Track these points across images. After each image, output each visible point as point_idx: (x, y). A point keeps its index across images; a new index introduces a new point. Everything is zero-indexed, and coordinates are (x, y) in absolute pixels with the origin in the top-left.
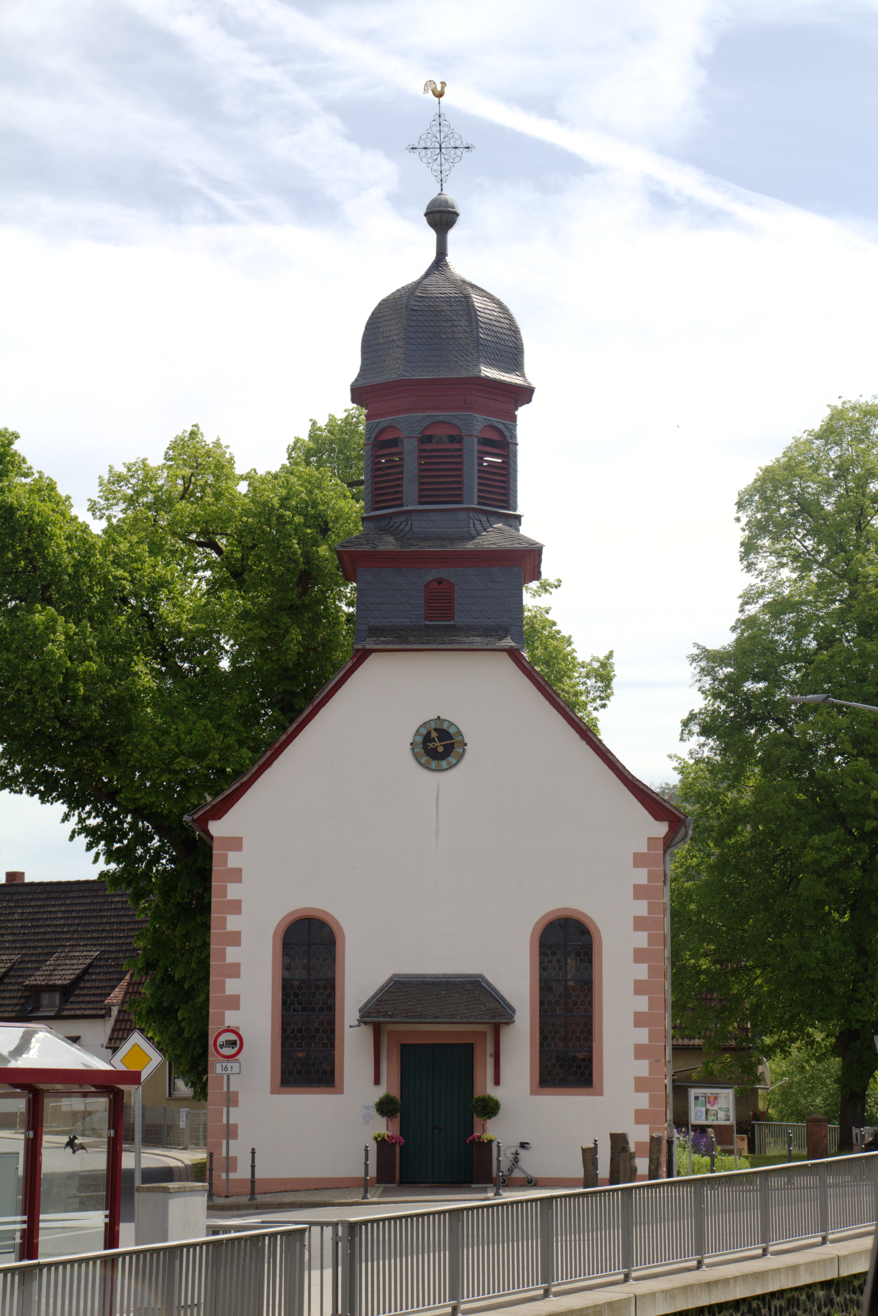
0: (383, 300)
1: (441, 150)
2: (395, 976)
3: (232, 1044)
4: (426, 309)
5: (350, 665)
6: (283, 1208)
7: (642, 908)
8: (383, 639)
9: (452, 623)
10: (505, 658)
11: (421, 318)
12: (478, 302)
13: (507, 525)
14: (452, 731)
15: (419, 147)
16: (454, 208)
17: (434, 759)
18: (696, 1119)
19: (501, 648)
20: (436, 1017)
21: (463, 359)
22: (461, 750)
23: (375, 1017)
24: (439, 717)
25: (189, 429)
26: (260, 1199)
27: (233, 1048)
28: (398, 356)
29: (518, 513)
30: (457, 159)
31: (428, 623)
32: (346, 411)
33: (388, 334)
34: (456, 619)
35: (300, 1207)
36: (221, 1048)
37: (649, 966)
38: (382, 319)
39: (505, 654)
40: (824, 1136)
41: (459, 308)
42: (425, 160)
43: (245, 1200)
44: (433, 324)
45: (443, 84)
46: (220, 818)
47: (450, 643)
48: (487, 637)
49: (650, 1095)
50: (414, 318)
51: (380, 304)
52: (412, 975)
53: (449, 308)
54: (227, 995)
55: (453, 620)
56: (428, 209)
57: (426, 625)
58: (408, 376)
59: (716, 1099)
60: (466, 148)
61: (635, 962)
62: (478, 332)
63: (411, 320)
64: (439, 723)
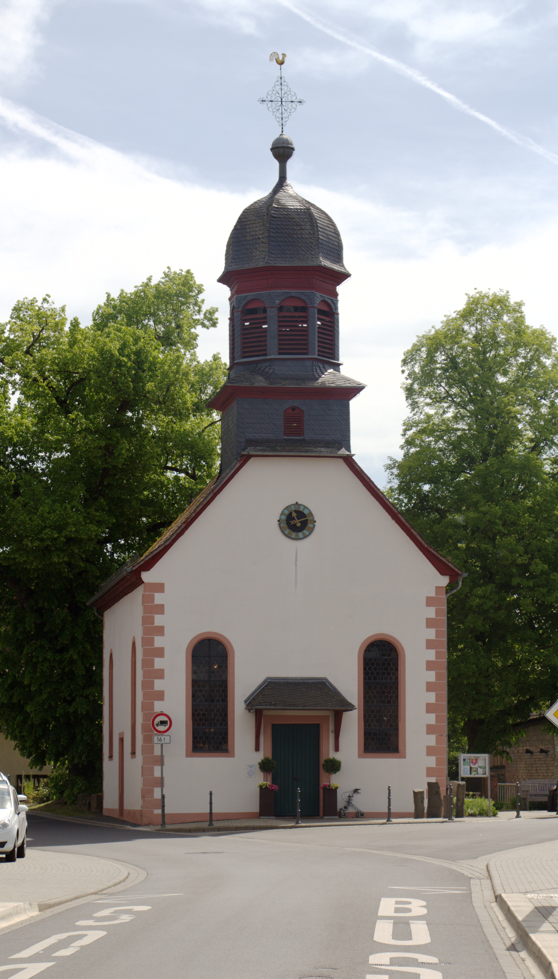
0: (246, 209)
1: (282, 103)
2: (268, 678)
3: (163, 723)
4: (282, 217)
5: (239, 465)
6: (240, 830)
7: (431, 634)
8: (258, 448)
9: (302, 438)
10: (341, 462)
11: (279, 223)
12: (316, 214)
13: (336, 371)
14: (306, 512)
15: (267, 100)
16: (292, 145)
17: (294, 531)
18: (464, 774)
19: (340, 455)
20: (304, 706)
21: (309, 253)
22: (312, 526)
23: (264, 705)
24: (297, 503)
25: (30, 298)
26: (216, 824)
27: (165, 726)
28: (263, 249)
29: (339, 362)
30: (293, 110)
31: (286, 437)
32: (136, 287)
33: (254, 234)
34: (305, 435)
35: (253, 829)
36: (157, 726)
37: (436, 673)
38: (248, 223)
39: (341, 460)
40: (495, 787)
41: (305, 217)
42: (271, 109)
43: (206, 825)
44: (287, 227)
45: (284, 55)
46: (149, 570)
47: (306, 452)
48: (329, 447)
49: (436, 758)
50: (274, 223)
51: (244, 212)
52: (280, 678)
53: (297, 217)
54: (156, 691)
55: (303, 435)
56: (273, 145)
57: (285, 439)
58: (272, 264)
59: (476, 760)
60: (299, 102)
61: (427, 670)
62: (319, 235)
63: (272, 224)
64: (297, 507)
